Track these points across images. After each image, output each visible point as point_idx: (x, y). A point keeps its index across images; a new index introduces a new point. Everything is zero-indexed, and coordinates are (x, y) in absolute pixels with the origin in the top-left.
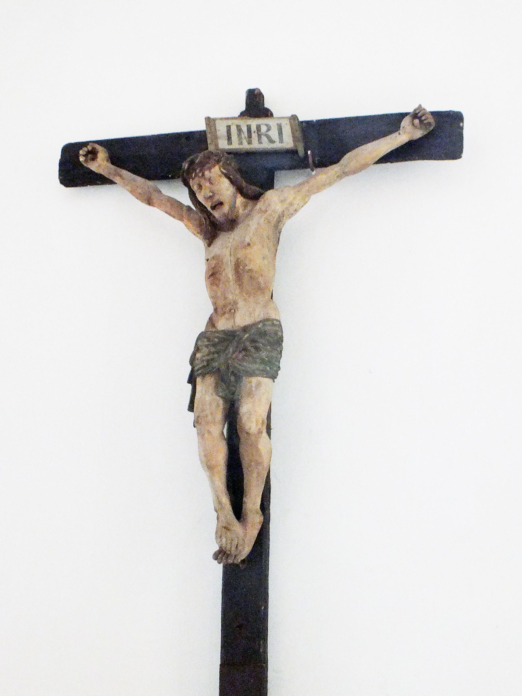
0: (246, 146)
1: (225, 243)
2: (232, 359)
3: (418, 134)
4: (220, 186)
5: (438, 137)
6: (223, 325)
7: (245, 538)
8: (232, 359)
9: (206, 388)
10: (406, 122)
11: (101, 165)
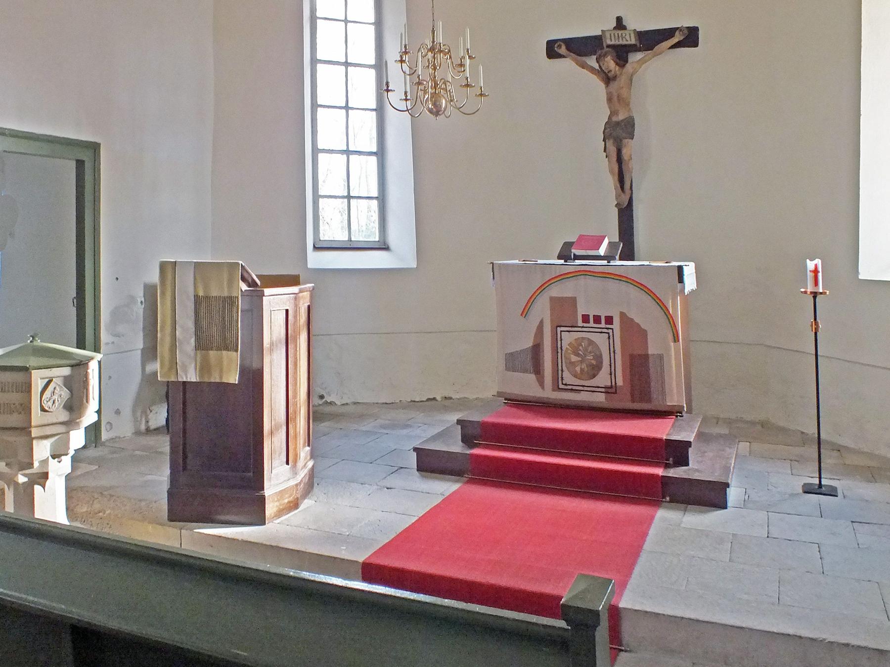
0: (617, 43)
1: (614, 86)
2: (619, 132)
3: (682, 38)
4: (610, 63)
5: (691, 38)
6: (614, 119)
7: (625, 200)
8: (619, 132)
9: (610, 143)
10: (677, 33)
11: (563, 50)
